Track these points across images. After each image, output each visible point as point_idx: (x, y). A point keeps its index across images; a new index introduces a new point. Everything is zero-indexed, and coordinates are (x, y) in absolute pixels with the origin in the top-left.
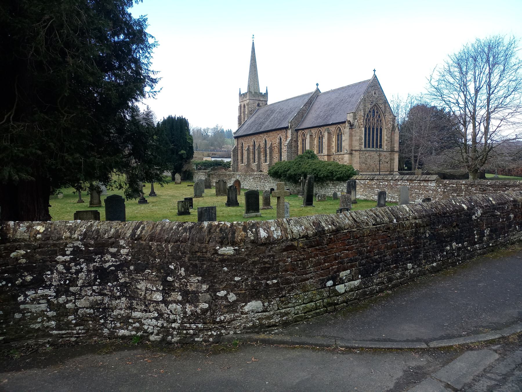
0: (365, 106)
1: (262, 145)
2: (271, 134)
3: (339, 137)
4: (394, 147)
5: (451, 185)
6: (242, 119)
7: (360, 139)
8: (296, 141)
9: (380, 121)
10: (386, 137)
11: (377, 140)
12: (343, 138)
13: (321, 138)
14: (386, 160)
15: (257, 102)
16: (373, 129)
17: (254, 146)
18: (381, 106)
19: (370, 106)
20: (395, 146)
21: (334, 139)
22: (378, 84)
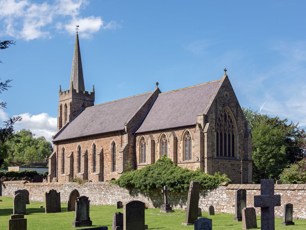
1: (90, 152)
6: (63, 121)
8: (134, 147)
10: (238, 145)
11: (229, 147)
17: (79, 152)
22: (229, 85)
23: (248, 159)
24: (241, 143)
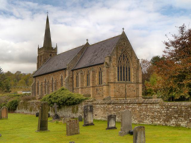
0: (117, 52)
1: (50, 82)
2: (55, 73)
3: (100, 73)
4: (139, 80)
5: (173, 107)
7: (114, 75)
8: (72, 78)
9: (129, 62)
10: (133, 74)
12: (103, 74)
13: (88, 75)
14: (133, 89)
15: (50, 54)
16: (124, 68)
18: (129, 53)
19: (120, 52)
20: (139, 79)
21: (96, 76)
22: (104, 42)
23: (139, 82)
24: (135, 73)
